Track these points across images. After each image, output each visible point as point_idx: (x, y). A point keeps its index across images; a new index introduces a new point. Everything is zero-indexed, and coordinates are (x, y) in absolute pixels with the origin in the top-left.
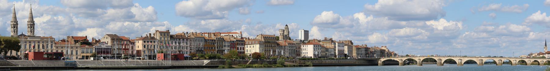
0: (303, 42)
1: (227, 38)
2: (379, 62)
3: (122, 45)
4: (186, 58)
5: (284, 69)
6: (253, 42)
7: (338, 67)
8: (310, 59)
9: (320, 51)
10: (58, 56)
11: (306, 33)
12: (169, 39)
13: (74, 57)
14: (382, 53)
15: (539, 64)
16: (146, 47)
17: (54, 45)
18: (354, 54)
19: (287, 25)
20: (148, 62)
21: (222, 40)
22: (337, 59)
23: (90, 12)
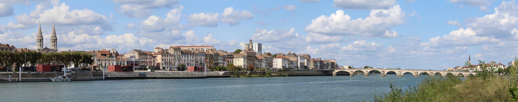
1: (220, 53)
2: (334, 73)
3: (147, 58)
8: (280, 70)
15: (463, 76)
21: (217, 55)
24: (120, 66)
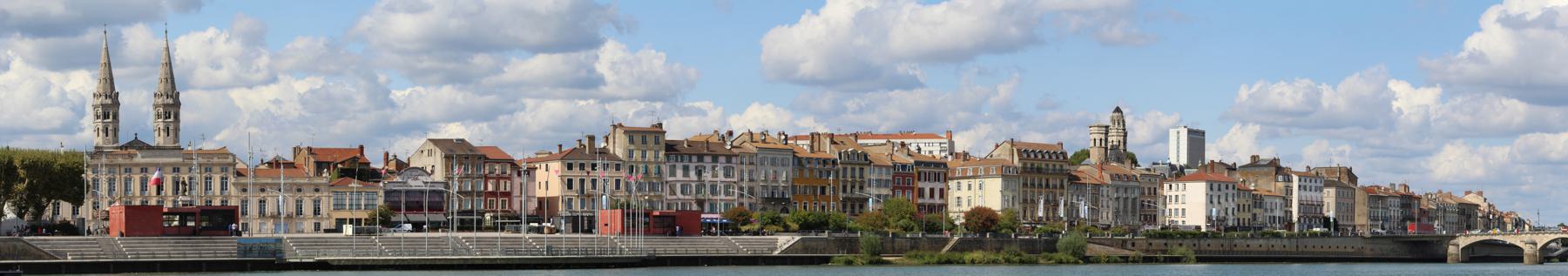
0: (1178, 173)
1: (878, 150)
2: (1451, 249)
3: (486, 178)
4: (708, 228)
5: (1083, 269)
6: (978, 168)
7: (1296, 266)
8: (1195, 234)
9: (1231, 205)
10: (221, 220)
11: (1197, 140)
12: (662, 154)
13: (308, 225)
14: (1466, 215)
16: (576, 185)
17: (232, 179)
18: (1361, 219)
19: (1118, 110)
20: (568, 241)
21: (864, 160)
22: (1290, 237)
23: (451, 66)
24: (159, 208)
